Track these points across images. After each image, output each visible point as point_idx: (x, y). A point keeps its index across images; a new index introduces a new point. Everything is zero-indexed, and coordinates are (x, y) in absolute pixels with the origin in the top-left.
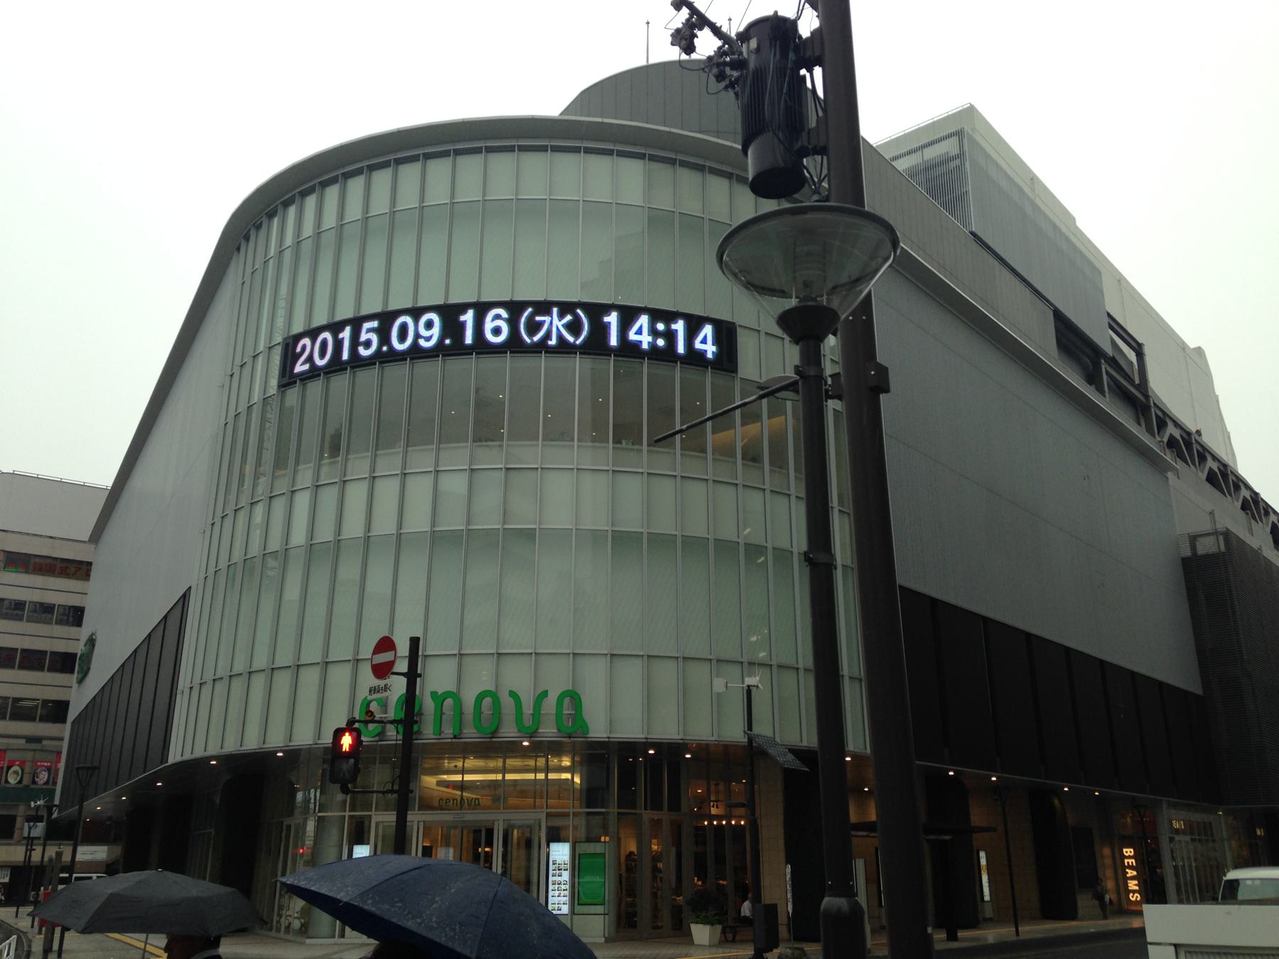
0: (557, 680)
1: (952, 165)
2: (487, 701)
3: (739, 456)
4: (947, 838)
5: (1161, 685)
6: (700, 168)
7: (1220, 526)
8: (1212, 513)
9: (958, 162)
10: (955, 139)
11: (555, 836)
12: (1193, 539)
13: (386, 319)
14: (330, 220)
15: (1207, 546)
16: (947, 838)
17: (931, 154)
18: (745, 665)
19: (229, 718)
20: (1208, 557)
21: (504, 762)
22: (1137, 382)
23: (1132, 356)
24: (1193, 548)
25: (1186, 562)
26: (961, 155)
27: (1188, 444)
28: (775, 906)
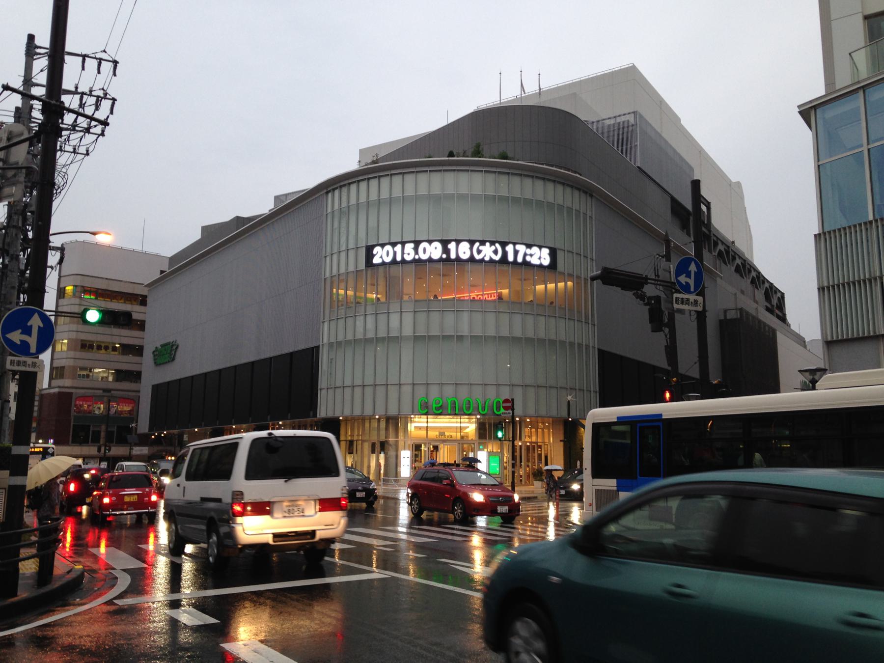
1: (631, 128)
7: (739, 306)
8: (735, 294)
12: (725, 311)
13: (417, 243)
15: (731, 315)
17: (619, 120)
19: (81, 386)
20: (731, 320)
21: (108, 409)
24: (725, 316)
25: (721, 321)
27: (727, 252)
28: (597, 490)
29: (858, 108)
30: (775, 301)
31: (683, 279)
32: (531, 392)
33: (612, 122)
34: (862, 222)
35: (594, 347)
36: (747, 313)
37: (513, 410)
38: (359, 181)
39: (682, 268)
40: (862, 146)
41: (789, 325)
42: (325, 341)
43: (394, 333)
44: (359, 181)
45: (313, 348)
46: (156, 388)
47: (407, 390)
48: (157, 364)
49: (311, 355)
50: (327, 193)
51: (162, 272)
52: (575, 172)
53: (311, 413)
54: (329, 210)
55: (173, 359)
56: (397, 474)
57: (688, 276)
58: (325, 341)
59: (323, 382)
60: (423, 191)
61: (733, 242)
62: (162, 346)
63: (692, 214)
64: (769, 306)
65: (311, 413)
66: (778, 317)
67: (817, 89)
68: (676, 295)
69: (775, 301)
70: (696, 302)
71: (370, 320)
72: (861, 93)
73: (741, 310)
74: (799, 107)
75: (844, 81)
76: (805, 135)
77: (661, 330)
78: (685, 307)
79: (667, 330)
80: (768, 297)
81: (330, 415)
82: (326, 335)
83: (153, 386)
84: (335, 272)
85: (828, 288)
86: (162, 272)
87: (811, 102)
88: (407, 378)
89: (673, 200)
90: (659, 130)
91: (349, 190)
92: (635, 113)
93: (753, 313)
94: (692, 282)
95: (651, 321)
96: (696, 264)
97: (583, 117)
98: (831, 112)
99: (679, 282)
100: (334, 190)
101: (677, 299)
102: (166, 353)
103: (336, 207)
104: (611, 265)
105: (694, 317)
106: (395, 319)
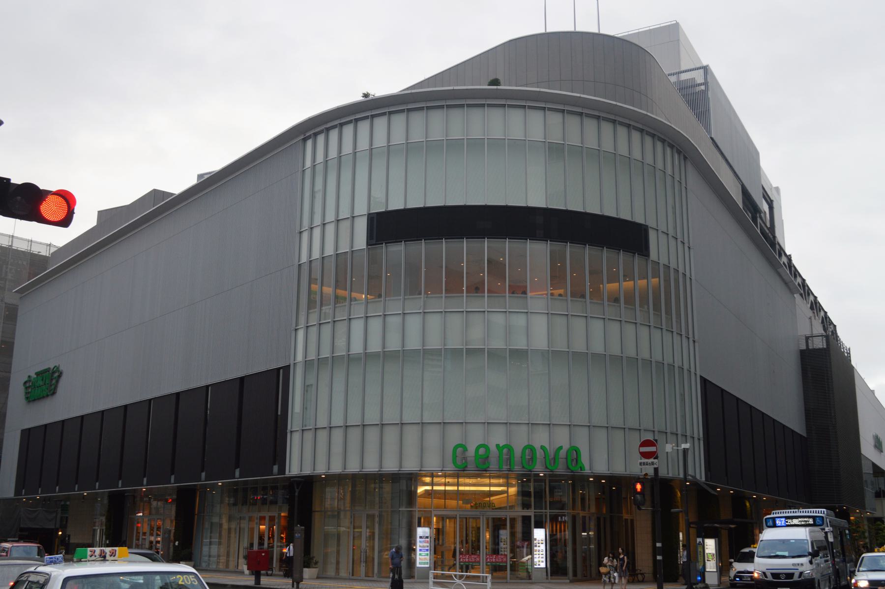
0: (562, 439)
2: (460, 450)
3: (606, 299)
4: (733, 526)
5: (793, 431)
6: (581, 114)
8: (810, 318)
9: (703, 87)
10: (702, 71)
11: (539, 525)
12: (807, 338)
14: (333, 153)
16: (733, 526)
18: (627, 430)
20: (815, 350)
22: (768, 225)
23: (765, 207)
26: (706, 84)
32: (602, 435)
38: (357, 120)
42: (300, 357)
44: (357, 120)
45: (278, 369)
46: (27, 434)
49: (276, 380)
50: (305, 140)
53: (276, 468)
54: (308, 163)
55: (54, 393)
56: (411, 563)
58: (300, 357)
59: (294, 422)
62: (37, 374)
65: (276, 468)
71: (375, 325)
81: (307, 471)
83: (23, 431)
84: (316, 255)
100: (316, 135)
102: (45, 384)
103: (320, 158)
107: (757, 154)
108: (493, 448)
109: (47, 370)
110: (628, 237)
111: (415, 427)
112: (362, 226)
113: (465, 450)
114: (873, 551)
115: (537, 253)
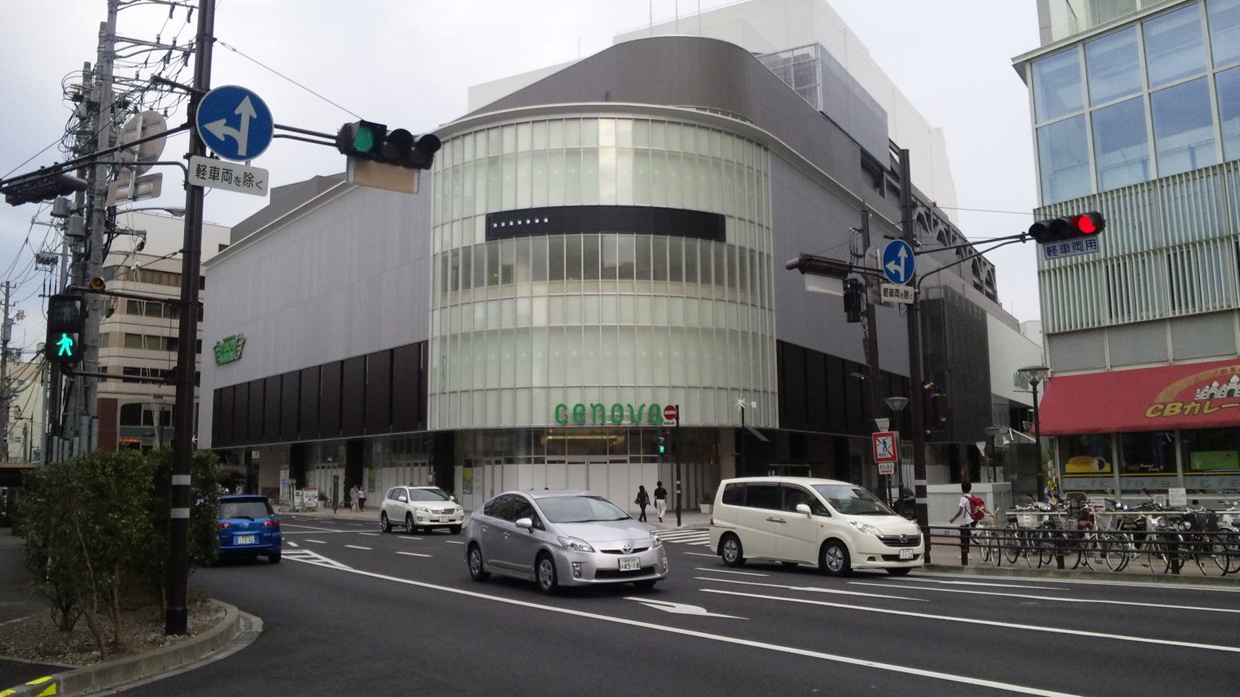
7: (943, 284)
17: (796, 53)
27: (928, 216)
29: (1077, 65)
30: (984, 276)
31: (892, 266)
33: (789, 55)
34: (1084, 195)
35: (771, 338)
36: (953, 292)
37: (677, 419)
39: (891, 254)
40: (1082, 107)
41: (1000, 305)
43: (523, 324)
45: (419, 344)
46: (219, 394)
47: (539, 396)
48: (219, 364)
49: (419, 350)
51: (222, 247)
52: (745, 119)
57: (898, 263)
59: (433, 385)
60: (556, 143)
61: (935, 205)
62: (225, 341)
63: (889, 175)
64: (977, 281)
66: (988, 295)
67: (1031, 42)
68: (884, 286)
69: (984, 276)
70: (906, 293)
72: (1080, 47)
73: (946, 288)
74: (1013, 59)
75: (1061, 32)
76: (1019, 93)
77: (858, 320)
78: (895, 300)
79: (865, 320)
80: (976, 271)
82: (436, 328)
85: (1049, 271)
86: (222, 247)
87: (1026, 54)
88: (537, 382)
89: (864, 154)
90: (844, 65)
91: (475, 141)
92: (815, 45)
93: (959, 290)
94: (901, 270)
95: (847, 309)
96: (906, 248)
97: (750, 49)
98: (1050, 67)
99: (887, 270)
101: (886, 290)
102: (231, 350)
104: (811, 251)
105: (904, 310)
106: (523, 306)
107: (884, 114)
108: (588, 407)
109: (234, 338)
110: (707, 226)
111: (510, 392)
112: (481, 224)
113: (566, 408)
114: (766, 475)
115: (618, 246)
